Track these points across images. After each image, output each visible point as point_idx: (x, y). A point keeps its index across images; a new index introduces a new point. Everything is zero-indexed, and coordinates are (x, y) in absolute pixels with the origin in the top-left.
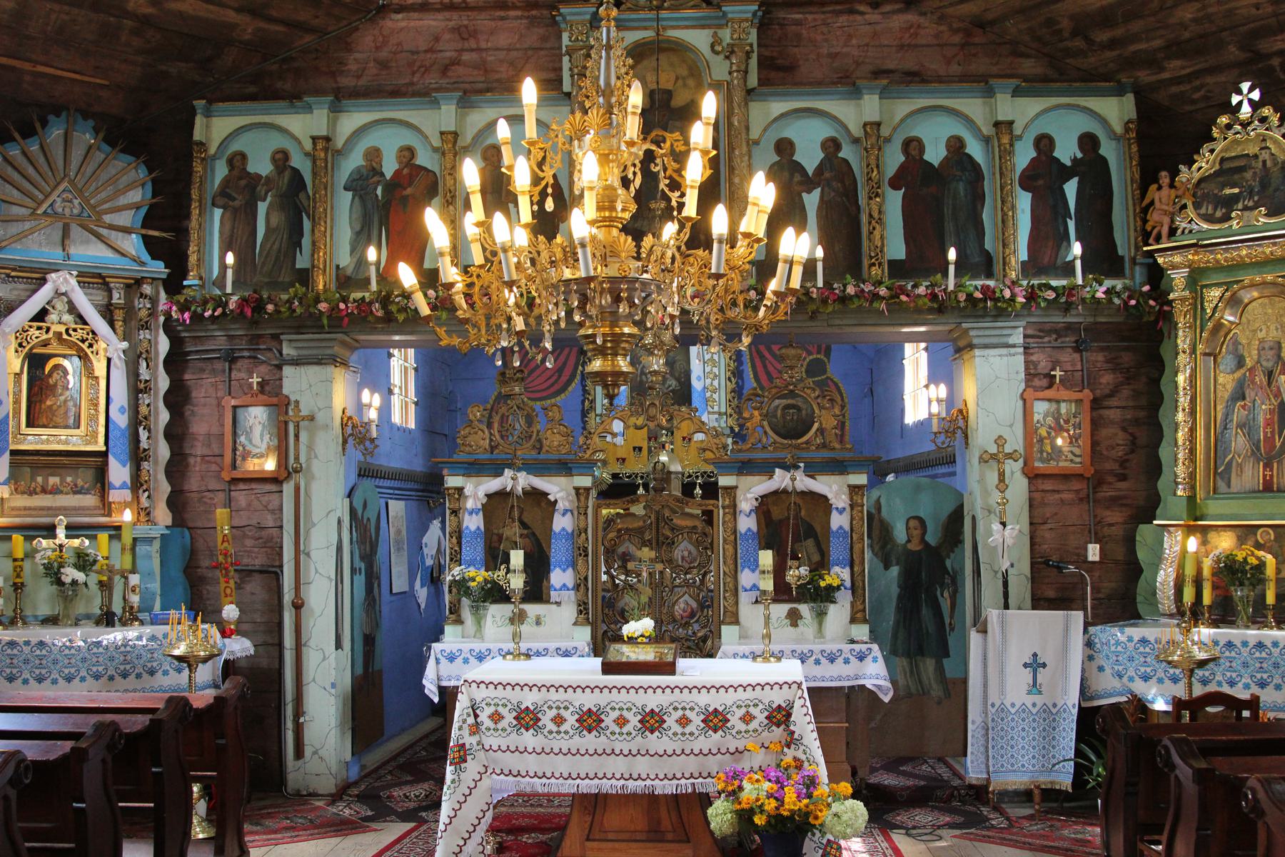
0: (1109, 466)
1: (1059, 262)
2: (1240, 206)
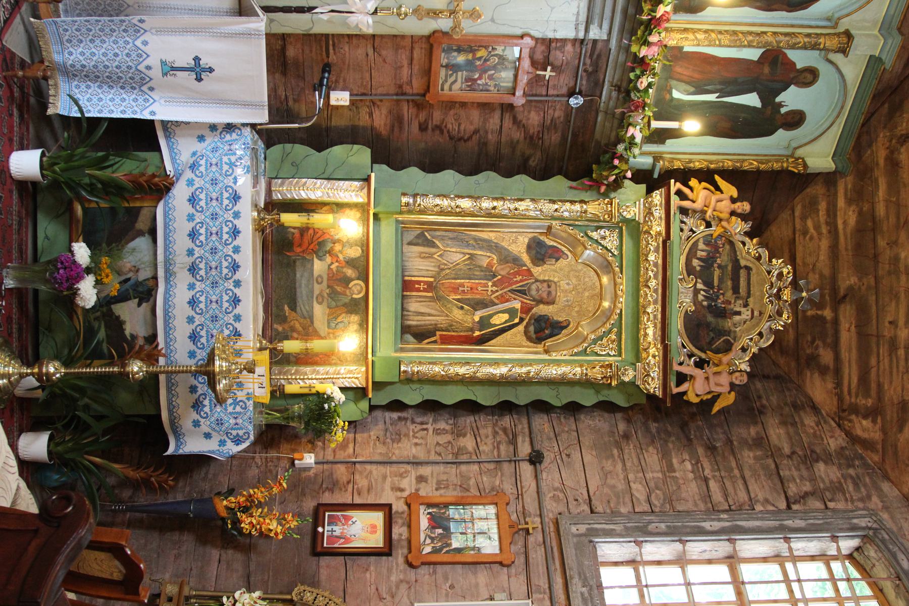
0: (437, 116)
1: (673, 83)
2: (700, 286)
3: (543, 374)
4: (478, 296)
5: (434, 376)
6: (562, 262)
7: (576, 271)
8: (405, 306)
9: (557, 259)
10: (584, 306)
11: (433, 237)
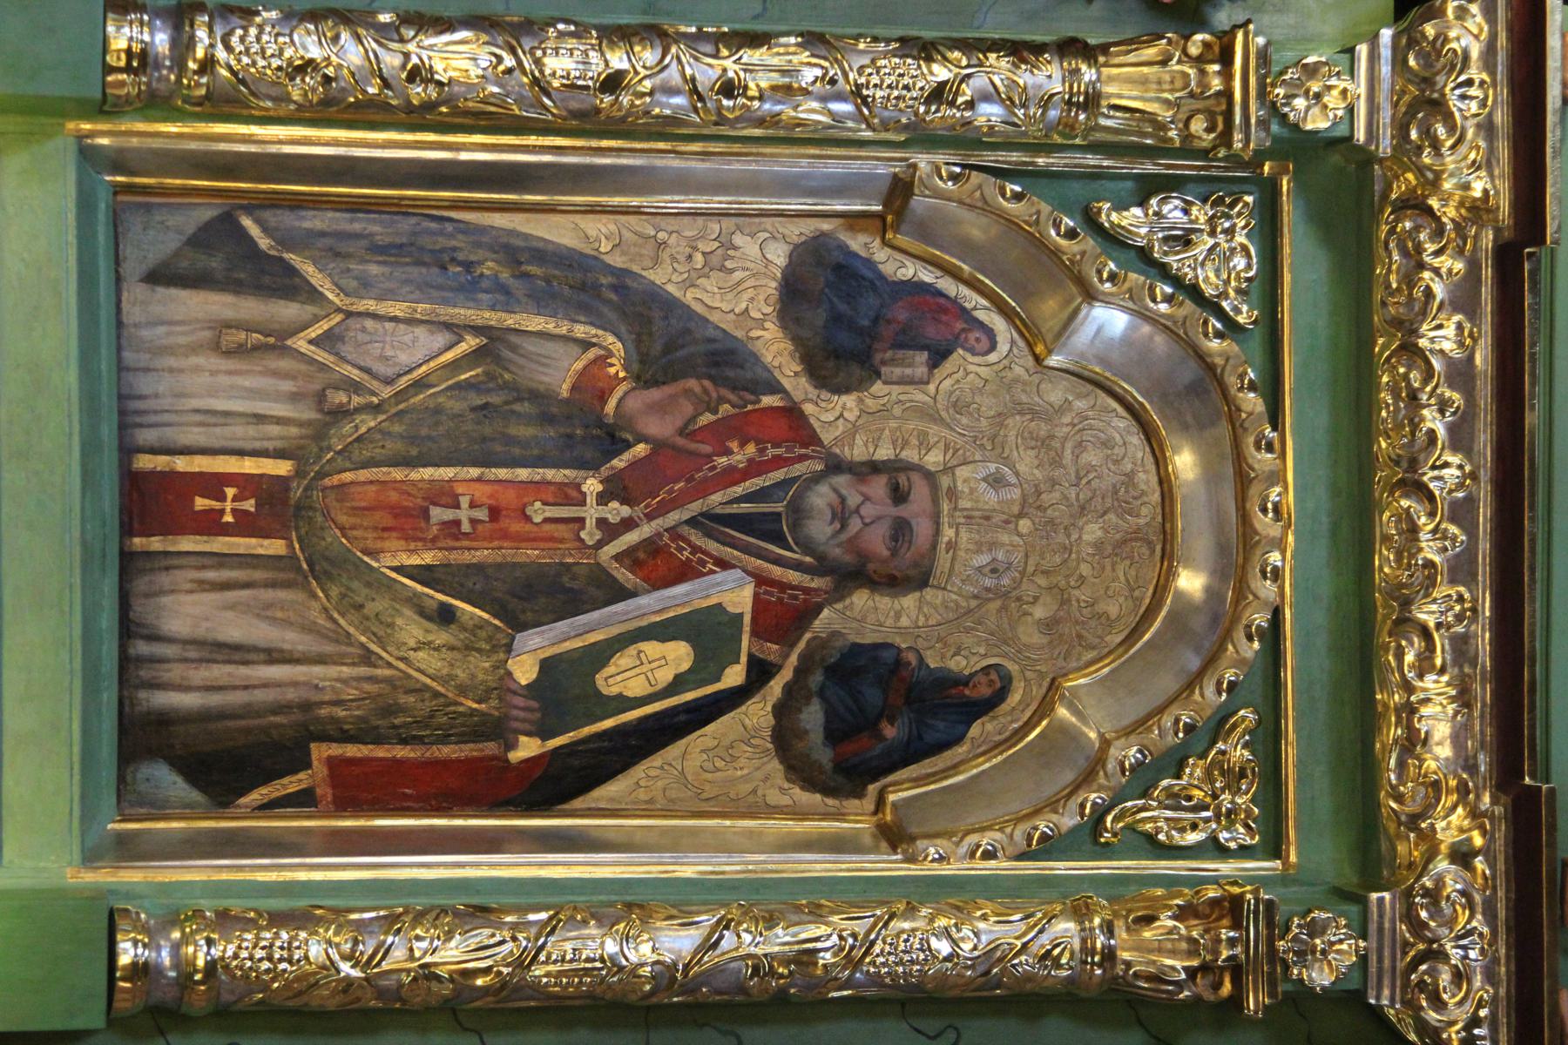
3: (881, 958)
4: (532, 553)
5: (308, 982)
6: (965, 370)
7: (1034, 414)
8: (139, 608)
9: (939, 356)
10: (1082, 595)
11: (287, 241)
